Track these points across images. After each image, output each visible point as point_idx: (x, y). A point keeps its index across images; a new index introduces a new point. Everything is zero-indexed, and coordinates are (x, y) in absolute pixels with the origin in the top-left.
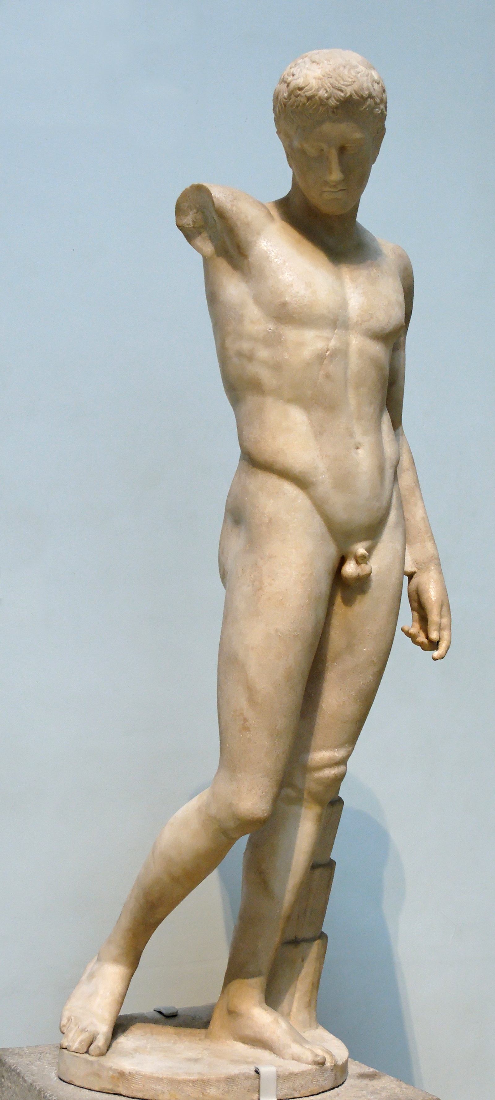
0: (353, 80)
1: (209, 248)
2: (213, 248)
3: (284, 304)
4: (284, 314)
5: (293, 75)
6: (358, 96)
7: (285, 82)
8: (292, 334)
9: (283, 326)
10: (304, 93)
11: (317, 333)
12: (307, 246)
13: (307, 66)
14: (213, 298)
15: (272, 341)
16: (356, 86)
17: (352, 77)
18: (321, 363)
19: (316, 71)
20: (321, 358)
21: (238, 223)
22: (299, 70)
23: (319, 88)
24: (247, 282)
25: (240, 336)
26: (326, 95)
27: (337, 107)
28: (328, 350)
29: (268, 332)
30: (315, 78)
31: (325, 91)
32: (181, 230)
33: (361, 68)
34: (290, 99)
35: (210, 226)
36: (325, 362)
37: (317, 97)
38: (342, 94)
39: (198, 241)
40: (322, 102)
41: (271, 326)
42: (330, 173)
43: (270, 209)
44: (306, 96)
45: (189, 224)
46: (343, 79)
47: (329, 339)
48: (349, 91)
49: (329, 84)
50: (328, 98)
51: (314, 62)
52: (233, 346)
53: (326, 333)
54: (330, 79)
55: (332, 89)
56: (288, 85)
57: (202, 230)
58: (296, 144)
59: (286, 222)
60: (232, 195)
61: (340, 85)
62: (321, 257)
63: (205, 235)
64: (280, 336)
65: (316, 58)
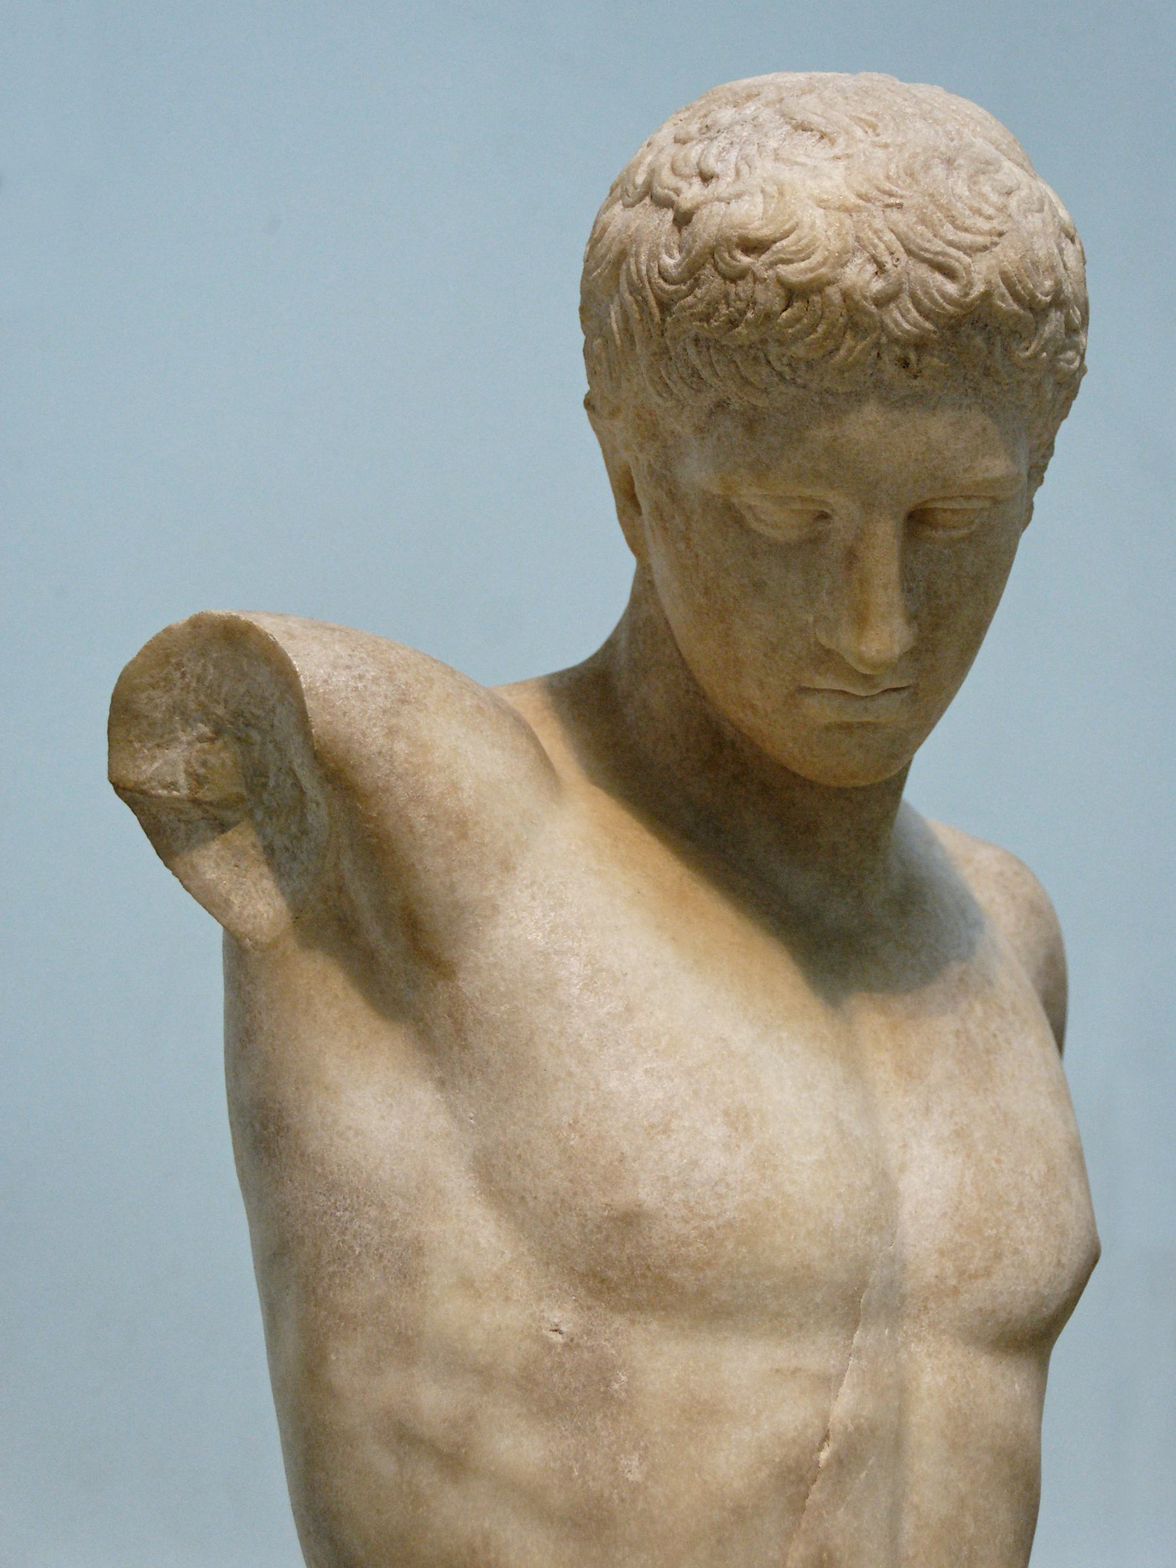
0: (995, 224)
1: (263, 904)
2: (280, 903)
3: (630, 1220)
4: (627, 1267)
5: (706, 178)
6: (1017, 297)
7: (663, 203)
8: (661, 1361)
9: (619, 1322)
10: (772, 265)
11: (781, 1354)
12: (716, 919)
13: (773, 144)
14: (266, 1132)
15: (571, 1391)
16: (1007, 255)
17: (991, 211)
18: (797, 1505)
19: (824, 170)
20: (796, 1480)
21: (418, 817)
22: (733, 155)
23: (844, 251)
24: (441, 1084)
25: (405, 1344)
26: (877, 285)
27: (920, 344)
28: (826, 1438)
29: (550, 1347)
30: (822, 204)
31: (871, 268)
32: (132, 804)
33: (1011, 172)
34: (697, 283)
35: (240, 764)
36: (816, 1495)
37: (833, 292)
38: (951, 288)
39: (212, 861)
40: (856, 316)
41: (563, 1316)
42: (861, 620)
43: (530, 716)
44: (780, 282)
45: (173, 785)
46: (953, 220)
47: (828, 1383)
48: (981, 272)
49: (889, 237)
50: (883, 301)
51: (804, 127)
52: (366, 1385)
53: (816, 1353)
54: (895, 215)
55: (904, 257)
56: (683, 220)
57: (228, 815)
58: (698, 472)
59: (608, 790)
60: (391, 679)
61: (938, 245)
62: (774, 971)
63: (243, 837)
64: (604, 1371)
65: (809, 108)
